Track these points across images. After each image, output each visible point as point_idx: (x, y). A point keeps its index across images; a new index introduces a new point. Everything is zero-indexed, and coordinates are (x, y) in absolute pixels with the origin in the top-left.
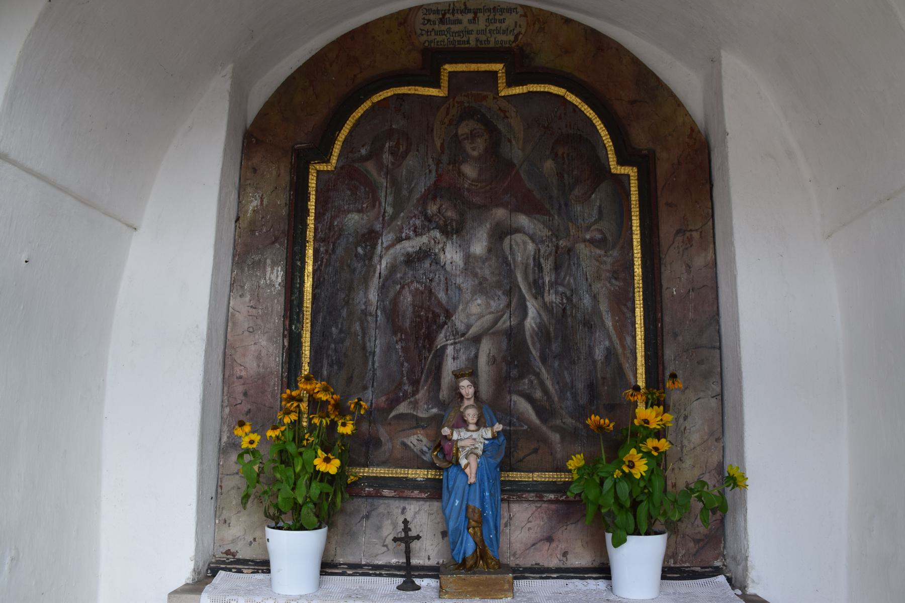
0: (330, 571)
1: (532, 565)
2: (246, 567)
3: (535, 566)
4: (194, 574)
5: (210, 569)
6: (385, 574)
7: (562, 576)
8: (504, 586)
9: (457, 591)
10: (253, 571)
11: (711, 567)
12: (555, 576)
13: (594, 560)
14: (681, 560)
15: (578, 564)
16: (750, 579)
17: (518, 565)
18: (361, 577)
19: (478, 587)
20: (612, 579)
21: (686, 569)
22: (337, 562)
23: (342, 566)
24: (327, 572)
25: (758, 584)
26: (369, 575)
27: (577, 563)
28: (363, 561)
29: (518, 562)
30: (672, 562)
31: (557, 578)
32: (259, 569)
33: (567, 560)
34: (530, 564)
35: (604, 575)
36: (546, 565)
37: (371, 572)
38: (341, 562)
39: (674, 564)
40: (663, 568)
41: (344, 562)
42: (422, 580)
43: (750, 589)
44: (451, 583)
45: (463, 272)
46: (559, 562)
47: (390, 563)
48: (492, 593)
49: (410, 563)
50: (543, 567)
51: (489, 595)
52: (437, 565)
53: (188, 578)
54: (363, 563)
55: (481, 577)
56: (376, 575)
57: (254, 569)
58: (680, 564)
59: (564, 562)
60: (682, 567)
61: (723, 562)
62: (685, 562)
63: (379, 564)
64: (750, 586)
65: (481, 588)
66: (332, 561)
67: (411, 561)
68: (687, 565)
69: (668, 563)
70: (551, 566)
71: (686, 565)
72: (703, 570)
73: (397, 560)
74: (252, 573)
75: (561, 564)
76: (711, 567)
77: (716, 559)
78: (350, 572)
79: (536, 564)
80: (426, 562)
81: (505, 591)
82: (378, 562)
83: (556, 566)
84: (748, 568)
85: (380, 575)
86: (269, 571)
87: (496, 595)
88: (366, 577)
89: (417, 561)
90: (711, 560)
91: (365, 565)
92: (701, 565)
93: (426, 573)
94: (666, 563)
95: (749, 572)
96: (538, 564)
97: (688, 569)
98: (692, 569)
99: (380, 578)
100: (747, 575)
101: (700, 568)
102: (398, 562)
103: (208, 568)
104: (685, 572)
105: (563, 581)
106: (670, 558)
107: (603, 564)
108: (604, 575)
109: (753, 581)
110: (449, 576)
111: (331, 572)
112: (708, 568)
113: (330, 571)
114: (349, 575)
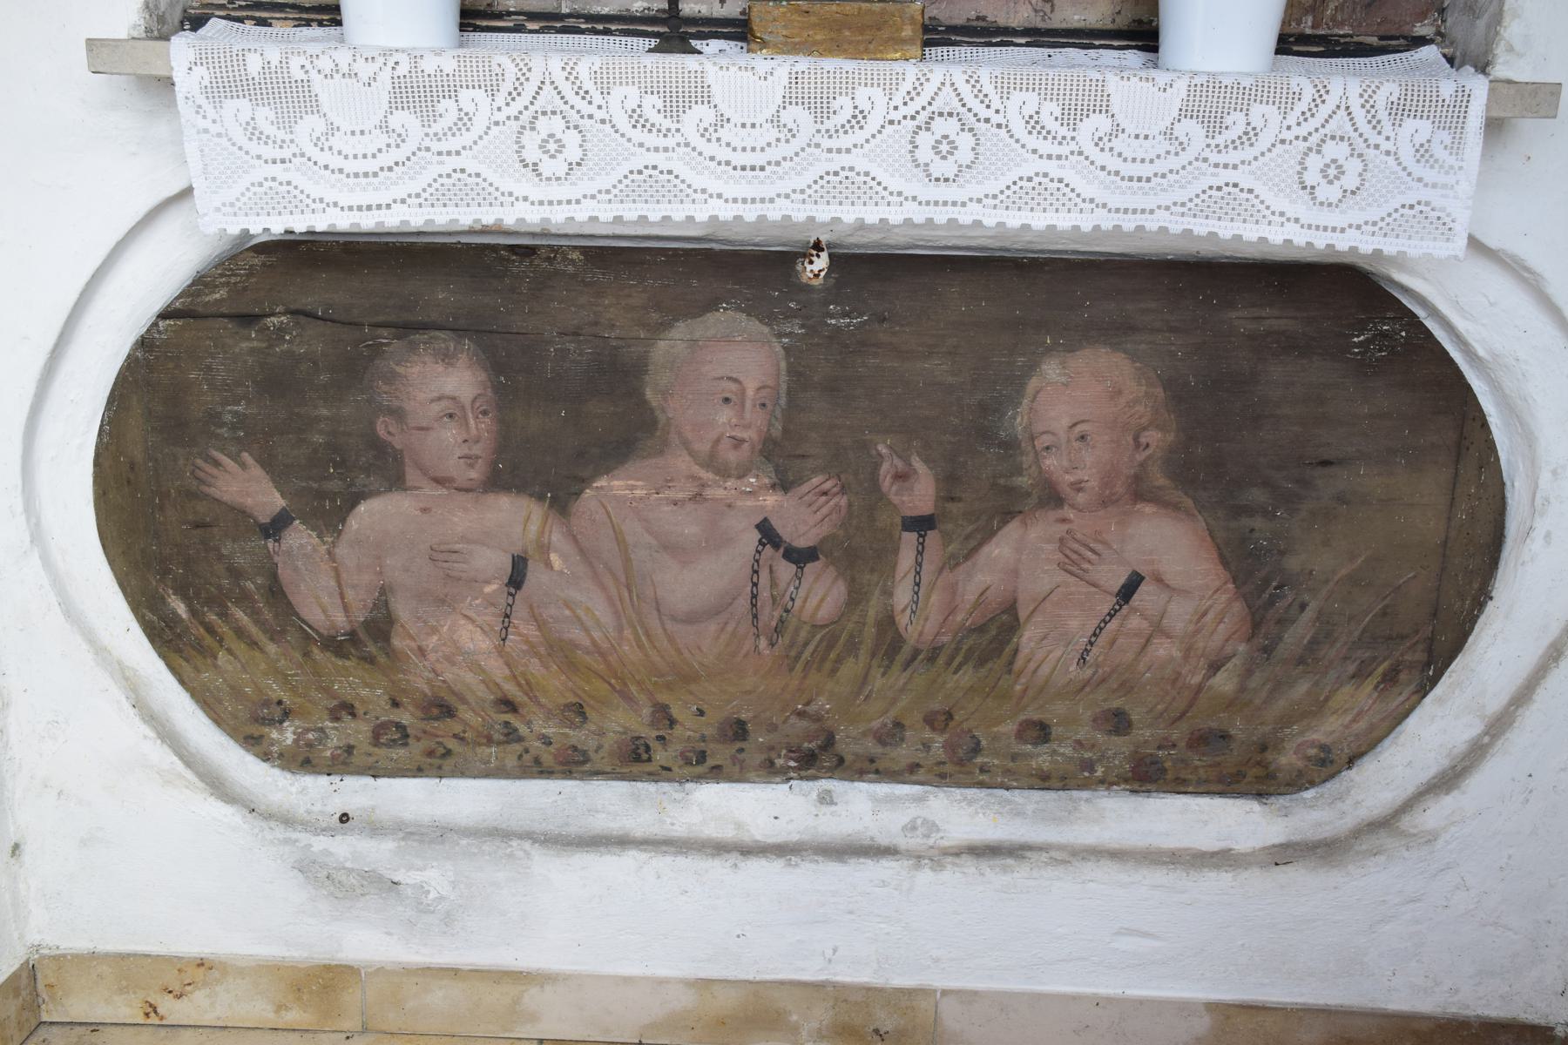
0: (484, 23)
1: (968, 19)
2: (278, 15)
3: (974, 24)
4: (147, 17)
5: (188, 20)
6: (617, 30)
7: (1037, 41)
8: (902, 29)
9: (789, 40)
10: (296, 23)
11: (1405, 38)
12: (1023, 41)
13: (1119, 13)
14: (1333, 18)
15: (1079, 21)
16: (1503, 43)
17: (935, 18)
18: (559, 36)
19: (839, 30)
20: (1160, 50)
21: (1342, 40)
22: (500, 8)
23: (513, 17)
24: (479, 27)
25: (1520, 55)
26: (582, 32)
27: (1076, 17)
28: (563, 5)
29: (935, 11)
30: (1310, 24)
31: (1028, 45)
32: (312, 20)
33: (1052, 11)
34: (965, 17)
35: (1140, 44)
36: (1002, 21)
37: (583, 26)
38: (511, 9)
39: (1313, 27)
40: (1280, 35)
41: (518, 9)
42: (705, 42)
43: (1498, 67)
44: (775, 20)
45: (736, 865)
46: (1033, 14)
47: (628, 10)
48: (871, 46)
49: (678, 11)
50: (994, 25)
51: (866, 51)
52: (743, 17)
53: (135, 27)
54: (565, 10)
55: (848, 8)
56: (597, 32)
57: (300, 19)
58: (1329, 28)
59: (1045, 14)
60: (1332, 36)
61: (1439, 27)
62: (1341, 24)
63: (603, 12)
64: (1500, 60)
65: (847, 33)
66: (488, 5)
67: (680, 7)
68: (1346, 30)
69: (1299, 24)
70: (1013, 25)
71: (1341, 33)
72: (1384, 43)
73: (646, 5)
74: (295, 26)
75: (1039, 19)
76: (1405, 38)
77: (1422, 16)
78: (531, 26)
79: (978, 18)
80: (715, 10)
81: (904, 41)
82: (599, 9)
83: (1027, 25)
84: (1505, 15)
85: (607, 32)
86: (339, 23)
87: (881, 52)
88: (571, 36)
89: (692, 5)
90: (1408, 19)
91: (570, 16)
92: (1381, 33)
93: (714, 30)
94: (1293, 24)
95: (1505, 24)
96: (983, 18)
97: (1348, 40)
98: (1356, 39)
99: (606, 38)
100: (1497, 33)
101: (1376, 39)
102: (649, 9)
103: (184, 17)
104: (1337, 43)
105: (1040, 50)
106: (1306, 12)
107: (1140, 22)
108: (1140, 44)
109: (1510, 49)
110: (771, 4)
111: (487, 27)
112: (1397, 38)
113: (484, 23)
114: (531, 32)
